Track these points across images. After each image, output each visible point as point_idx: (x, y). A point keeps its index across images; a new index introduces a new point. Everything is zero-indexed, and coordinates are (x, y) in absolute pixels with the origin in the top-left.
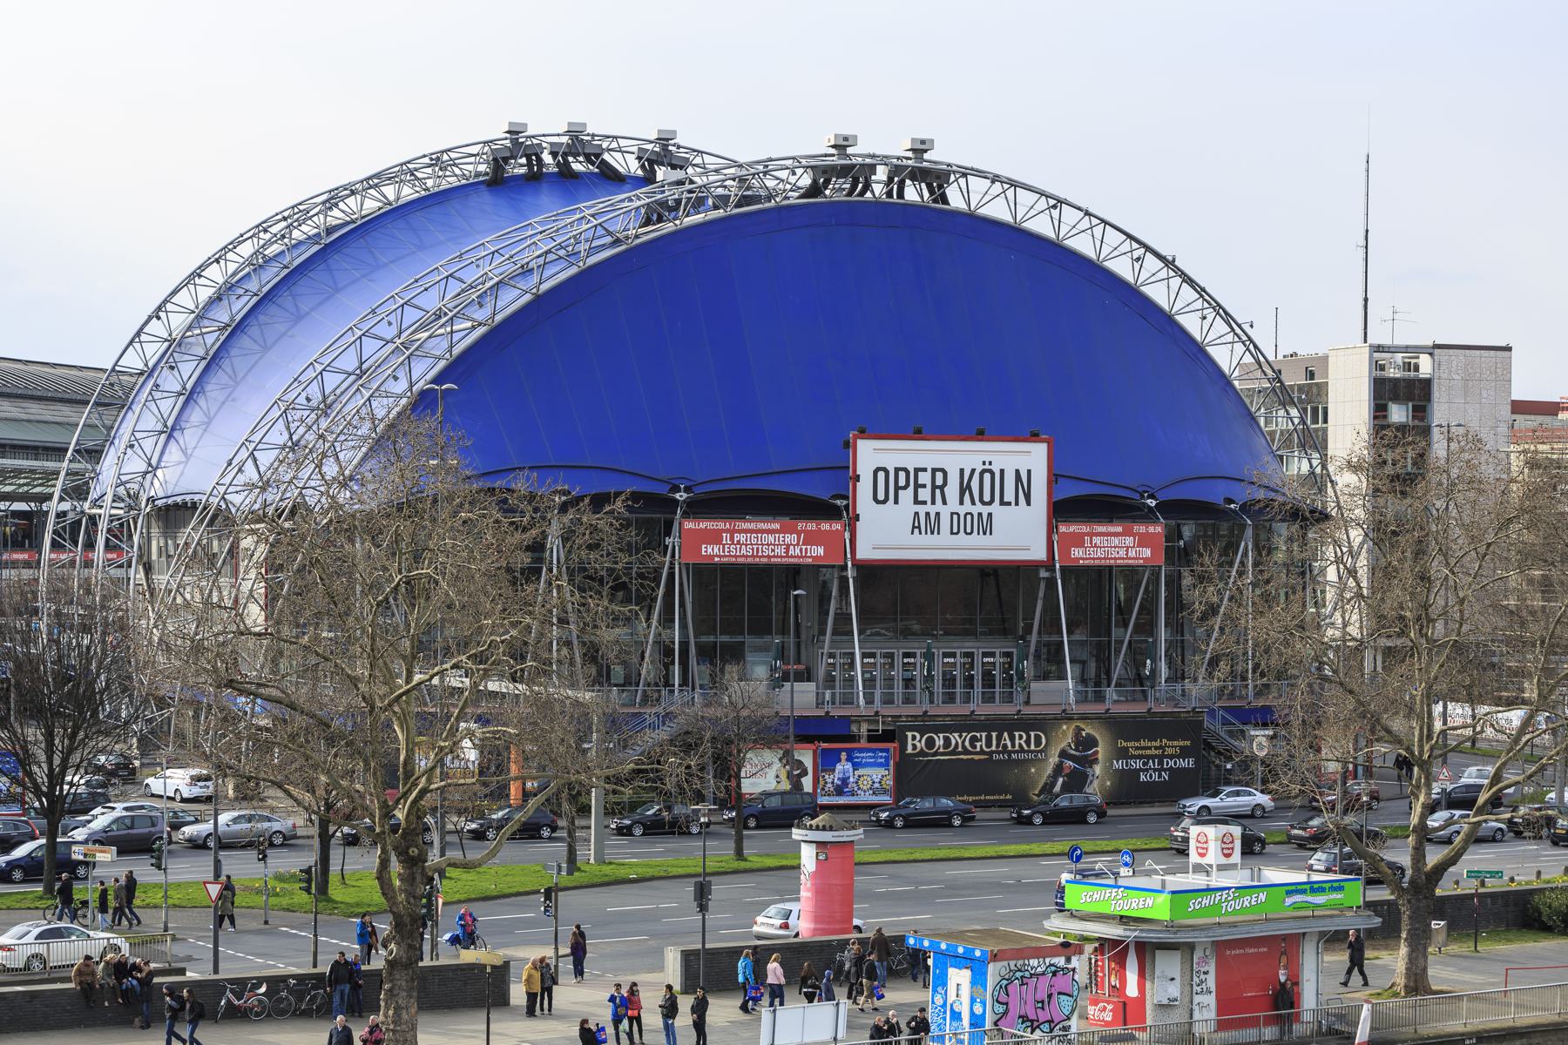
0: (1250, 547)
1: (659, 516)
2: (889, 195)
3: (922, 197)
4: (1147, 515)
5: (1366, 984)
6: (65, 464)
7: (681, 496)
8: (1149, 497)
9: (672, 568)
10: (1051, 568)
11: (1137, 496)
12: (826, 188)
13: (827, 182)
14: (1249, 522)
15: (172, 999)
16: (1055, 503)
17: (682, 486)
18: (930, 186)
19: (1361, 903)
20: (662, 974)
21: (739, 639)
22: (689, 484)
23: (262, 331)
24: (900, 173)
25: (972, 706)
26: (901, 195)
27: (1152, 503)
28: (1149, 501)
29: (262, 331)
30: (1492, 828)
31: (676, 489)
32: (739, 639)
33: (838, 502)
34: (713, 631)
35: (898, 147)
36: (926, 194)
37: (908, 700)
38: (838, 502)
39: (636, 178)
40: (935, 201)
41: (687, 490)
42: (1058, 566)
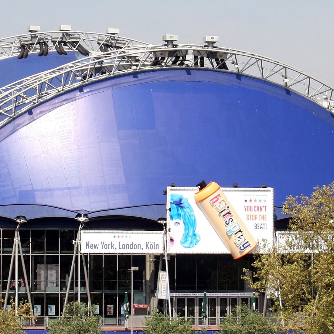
1: (73, 229)
2: (196, 64)
3: (213, 66)
7: (82, 219)
9: (77, 257)
12: (163, 62)
13: (163, 58)
15: (122, 269)
17: (83, 214)
18: (217, 60)
20: (147, 259)
21: (132, 271)
23: (33, 188)
24: (199, 56)
25: (203, 326)
26: (202, 64)
29: (33, 188)
31: (79, 215)
32: (132, 271)
33: (161, 222)
34: (99, 288)
35: (199, 46)
36: (215, 64)
37: (165, 286)
38: (161, 222)
39: (68, 43)
40: (220, 68)
41: (86, 215)
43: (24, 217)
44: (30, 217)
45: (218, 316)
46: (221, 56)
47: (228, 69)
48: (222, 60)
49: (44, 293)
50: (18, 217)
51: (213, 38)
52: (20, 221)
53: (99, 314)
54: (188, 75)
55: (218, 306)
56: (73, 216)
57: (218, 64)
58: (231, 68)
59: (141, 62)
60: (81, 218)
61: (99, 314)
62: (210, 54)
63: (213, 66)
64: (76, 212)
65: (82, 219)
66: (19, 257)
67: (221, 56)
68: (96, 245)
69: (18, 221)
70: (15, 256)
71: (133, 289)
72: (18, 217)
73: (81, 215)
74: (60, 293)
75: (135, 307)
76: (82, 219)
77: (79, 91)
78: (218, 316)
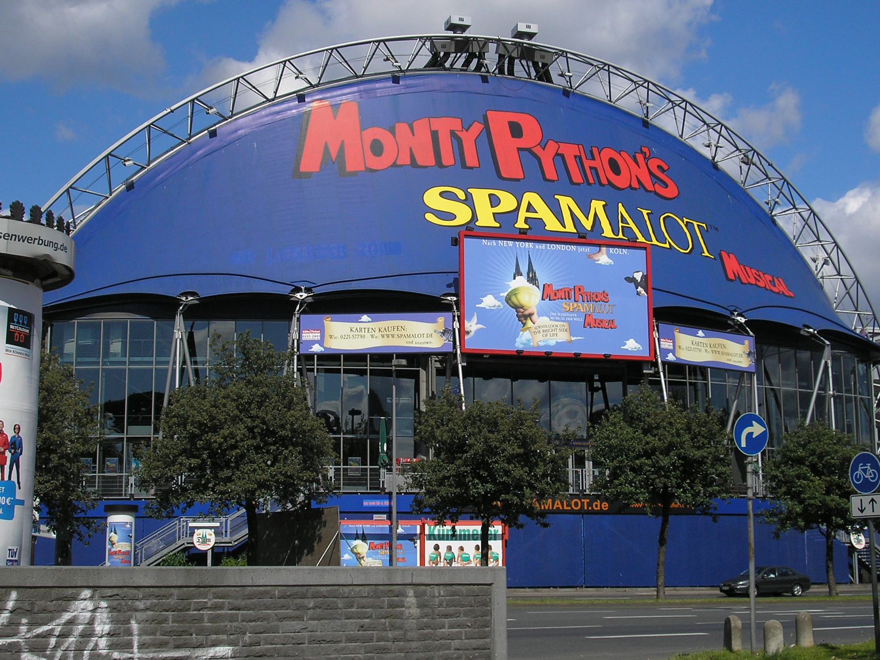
0: (830, 365)
3: (529, 74)
4: (738, 330)
5: (653, 289)
6: (368, 467)
8: (739, 315)
10: (655, 365)
11: (727, 313)
14: (827, 342)
16: (655, 309)
18: (535, 64)
19: (363, 169)
22: (309, 285)
27: (742, 320)
28: (739, 318)
30: (154, 602)
31: (298, 290)
36: (533, 74)
40: (540, 79)
41: (308, 290)
42: (660, 361)
43: (193, 294)
44: (204, 293)
45: (589, 467)
46: (543, 57)
47: (551, 82)
48: (545, 65)
49: (124, 438)
50: (183, 294)
51: (529, 27)
52: (187, 298)
53: (17, 498)
54: (513, 139)
55: (588, 460)
56: (285, 290)
57: (537, 72)
58: (558, 81)
59: (645, 474)
60: (301, 294)
61: (17, 498)
62: (524, 50)
63: (529, 74)
64: (293, 284)
65: (301, 296)
66: (182, 371)
67: (543, 57)
68: (22, 237)
69: (184, 299)
70: (174, 371)
71: (370, 375)
72: (186, 294)
73: (301, 289)
74: (152, 436)
75: (401, 462)
76: (301, 296)
77: (784, 632)
78: (589, 467)
